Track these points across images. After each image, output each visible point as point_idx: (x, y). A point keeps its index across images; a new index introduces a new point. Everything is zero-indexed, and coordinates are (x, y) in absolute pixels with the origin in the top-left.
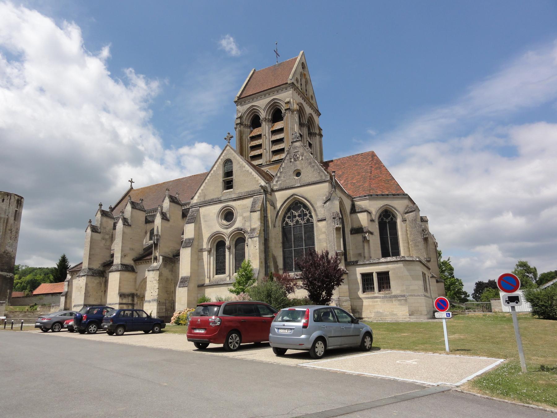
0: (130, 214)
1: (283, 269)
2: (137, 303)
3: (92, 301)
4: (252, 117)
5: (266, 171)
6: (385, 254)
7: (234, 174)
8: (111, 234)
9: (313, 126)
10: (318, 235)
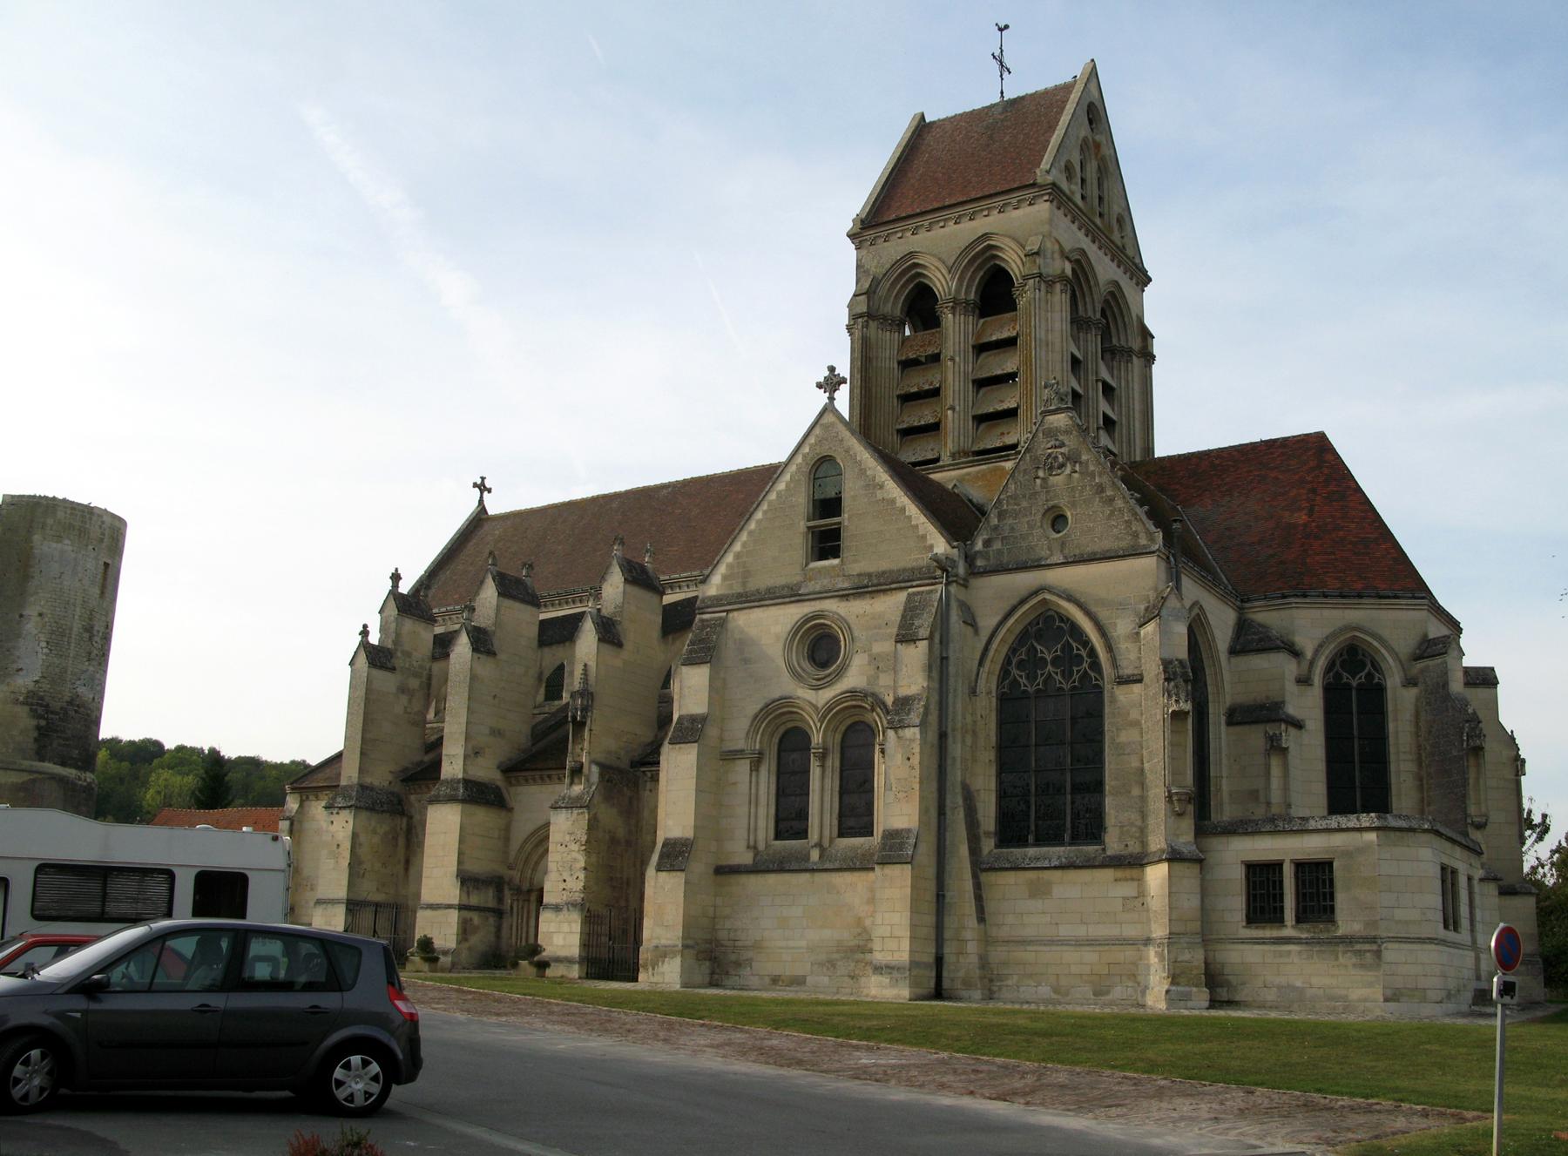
0: (492, 613)
1: (996, 834)
2: (512, 908)
4: (910, 291)
5: (950, 487)
6: (1341, 800)
7: (846, 510)
8: (425, 673)
10: (1114, 729)
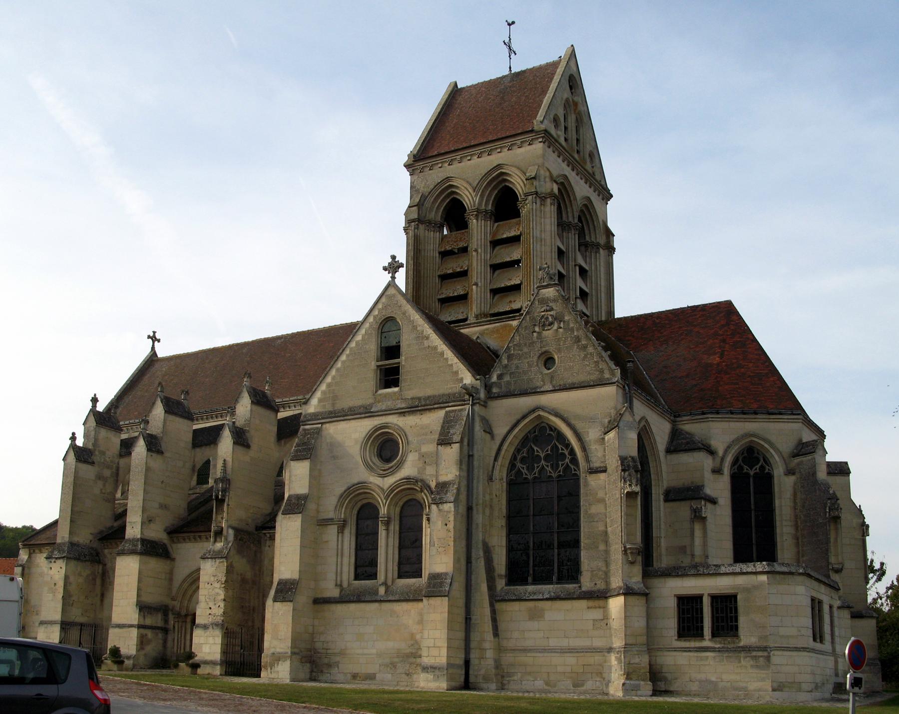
0: (161, 425)
2: (174, 627)
3: (77, 615)
5: (475, 338)
7: (404, 354)
9: (591, 226)
